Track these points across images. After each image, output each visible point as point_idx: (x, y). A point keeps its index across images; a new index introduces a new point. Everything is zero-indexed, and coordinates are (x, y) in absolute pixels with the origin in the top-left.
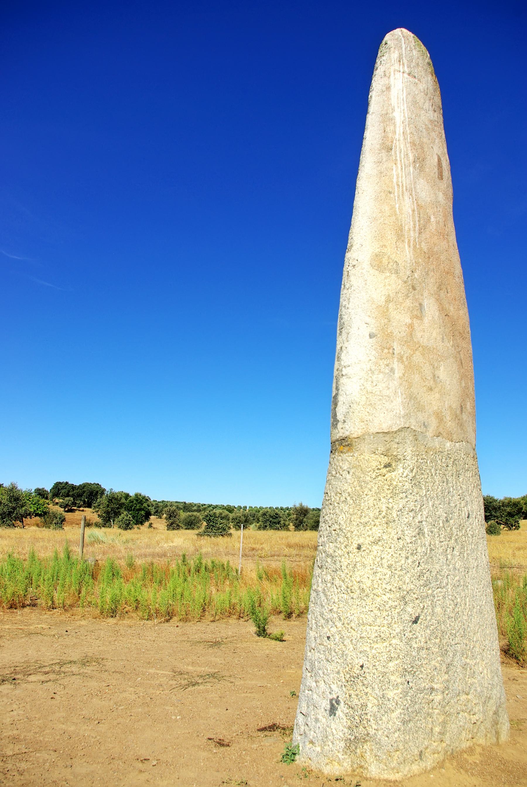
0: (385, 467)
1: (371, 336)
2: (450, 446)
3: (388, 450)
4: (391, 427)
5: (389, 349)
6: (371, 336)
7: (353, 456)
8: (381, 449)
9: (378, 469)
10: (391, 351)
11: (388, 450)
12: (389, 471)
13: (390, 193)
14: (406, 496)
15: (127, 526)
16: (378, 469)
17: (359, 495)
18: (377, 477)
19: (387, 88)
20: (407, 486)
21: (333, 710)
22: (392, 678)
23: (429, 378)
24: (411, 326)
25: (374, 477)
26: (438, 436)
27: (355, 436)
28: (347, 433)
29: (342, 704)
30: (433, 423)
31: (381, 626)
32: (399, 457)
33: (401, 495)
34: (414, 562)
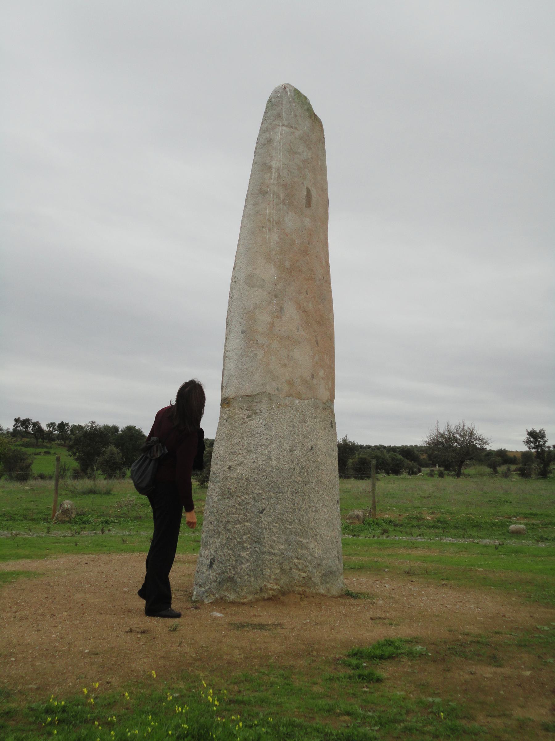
0: (248, 417)
1: (243, 332)
2: (299, 402)
3: (250, 407)
4: (252, 392)
5: (254, 341)
6: (243, 332)
7: (229, 410)
8: (246, 406)
9: (244, 419)
10: (255, 342)
11: (250, 407)
12: (251, 420)
13: (263, 227)
14: (260, 436)
15: (204, 480)
16: (244, 419)
17: (231, 435)
18: (242, 424)
19: (267, 141)
20: (261, 429)
21: (211, 566)
22: (245, 545)
23: (284, 358)
24: (272, 323)
25: (240, 423)
26: (289, 397)
27: (231, 397)
28: (227, 395)
29: (216, 561)
30: (286, 388)
31: (240, 514)
32: (257, 411)
33: (257, 435)
34: (263, 476)
